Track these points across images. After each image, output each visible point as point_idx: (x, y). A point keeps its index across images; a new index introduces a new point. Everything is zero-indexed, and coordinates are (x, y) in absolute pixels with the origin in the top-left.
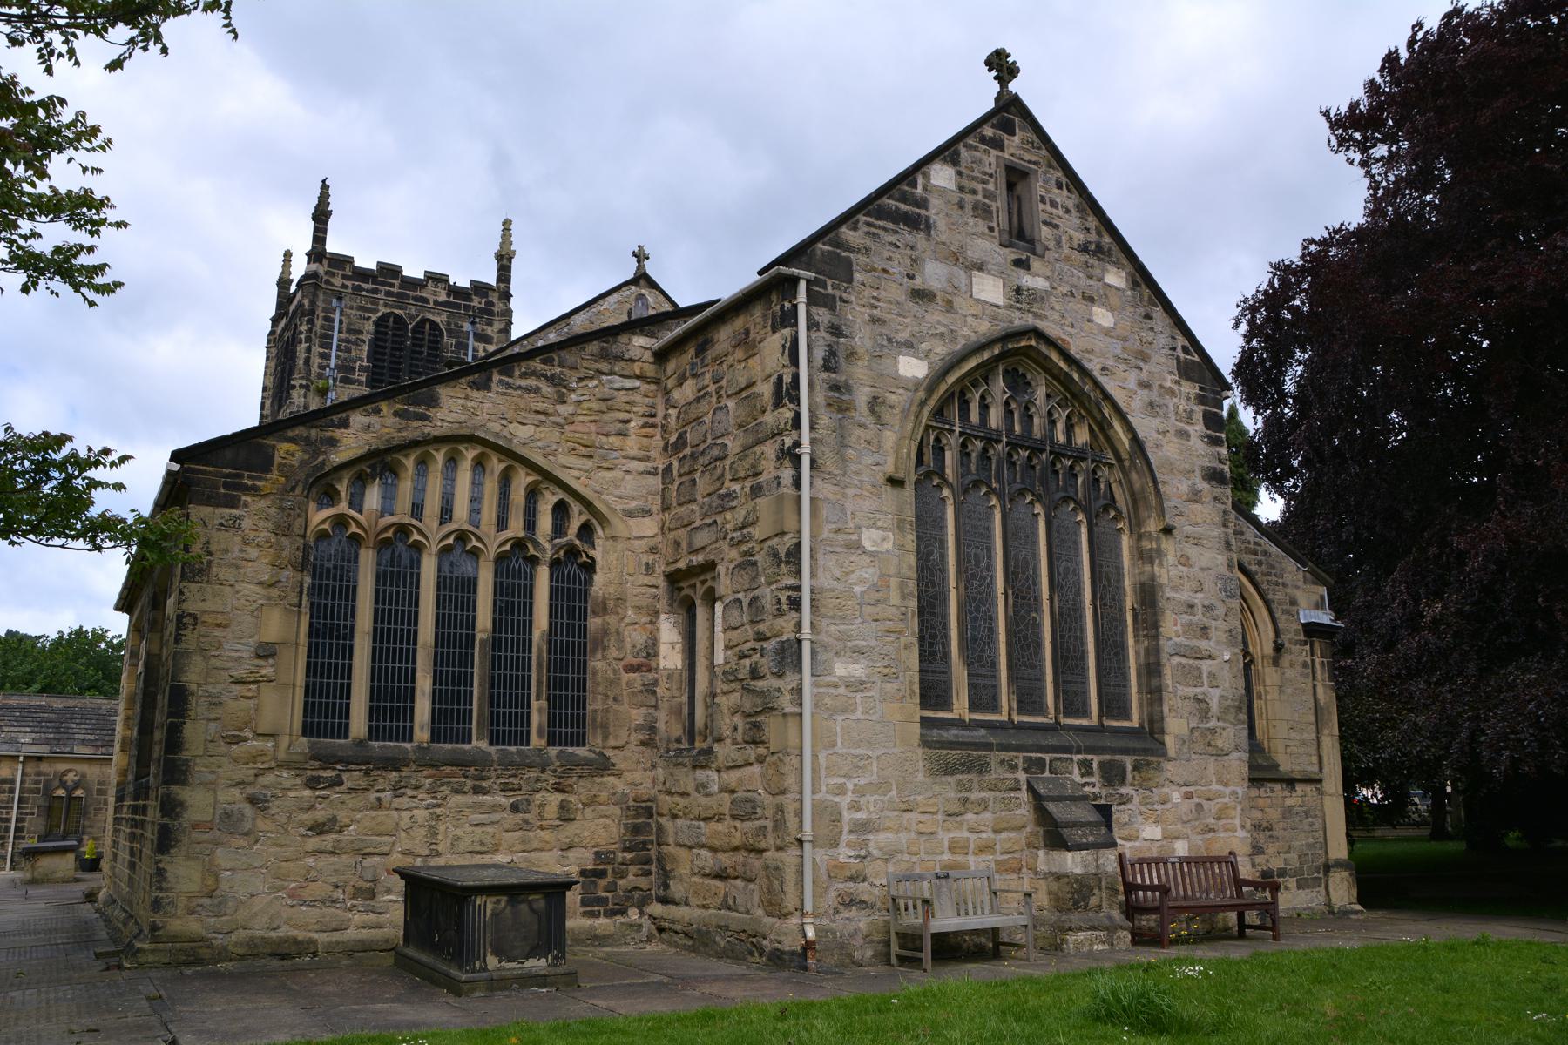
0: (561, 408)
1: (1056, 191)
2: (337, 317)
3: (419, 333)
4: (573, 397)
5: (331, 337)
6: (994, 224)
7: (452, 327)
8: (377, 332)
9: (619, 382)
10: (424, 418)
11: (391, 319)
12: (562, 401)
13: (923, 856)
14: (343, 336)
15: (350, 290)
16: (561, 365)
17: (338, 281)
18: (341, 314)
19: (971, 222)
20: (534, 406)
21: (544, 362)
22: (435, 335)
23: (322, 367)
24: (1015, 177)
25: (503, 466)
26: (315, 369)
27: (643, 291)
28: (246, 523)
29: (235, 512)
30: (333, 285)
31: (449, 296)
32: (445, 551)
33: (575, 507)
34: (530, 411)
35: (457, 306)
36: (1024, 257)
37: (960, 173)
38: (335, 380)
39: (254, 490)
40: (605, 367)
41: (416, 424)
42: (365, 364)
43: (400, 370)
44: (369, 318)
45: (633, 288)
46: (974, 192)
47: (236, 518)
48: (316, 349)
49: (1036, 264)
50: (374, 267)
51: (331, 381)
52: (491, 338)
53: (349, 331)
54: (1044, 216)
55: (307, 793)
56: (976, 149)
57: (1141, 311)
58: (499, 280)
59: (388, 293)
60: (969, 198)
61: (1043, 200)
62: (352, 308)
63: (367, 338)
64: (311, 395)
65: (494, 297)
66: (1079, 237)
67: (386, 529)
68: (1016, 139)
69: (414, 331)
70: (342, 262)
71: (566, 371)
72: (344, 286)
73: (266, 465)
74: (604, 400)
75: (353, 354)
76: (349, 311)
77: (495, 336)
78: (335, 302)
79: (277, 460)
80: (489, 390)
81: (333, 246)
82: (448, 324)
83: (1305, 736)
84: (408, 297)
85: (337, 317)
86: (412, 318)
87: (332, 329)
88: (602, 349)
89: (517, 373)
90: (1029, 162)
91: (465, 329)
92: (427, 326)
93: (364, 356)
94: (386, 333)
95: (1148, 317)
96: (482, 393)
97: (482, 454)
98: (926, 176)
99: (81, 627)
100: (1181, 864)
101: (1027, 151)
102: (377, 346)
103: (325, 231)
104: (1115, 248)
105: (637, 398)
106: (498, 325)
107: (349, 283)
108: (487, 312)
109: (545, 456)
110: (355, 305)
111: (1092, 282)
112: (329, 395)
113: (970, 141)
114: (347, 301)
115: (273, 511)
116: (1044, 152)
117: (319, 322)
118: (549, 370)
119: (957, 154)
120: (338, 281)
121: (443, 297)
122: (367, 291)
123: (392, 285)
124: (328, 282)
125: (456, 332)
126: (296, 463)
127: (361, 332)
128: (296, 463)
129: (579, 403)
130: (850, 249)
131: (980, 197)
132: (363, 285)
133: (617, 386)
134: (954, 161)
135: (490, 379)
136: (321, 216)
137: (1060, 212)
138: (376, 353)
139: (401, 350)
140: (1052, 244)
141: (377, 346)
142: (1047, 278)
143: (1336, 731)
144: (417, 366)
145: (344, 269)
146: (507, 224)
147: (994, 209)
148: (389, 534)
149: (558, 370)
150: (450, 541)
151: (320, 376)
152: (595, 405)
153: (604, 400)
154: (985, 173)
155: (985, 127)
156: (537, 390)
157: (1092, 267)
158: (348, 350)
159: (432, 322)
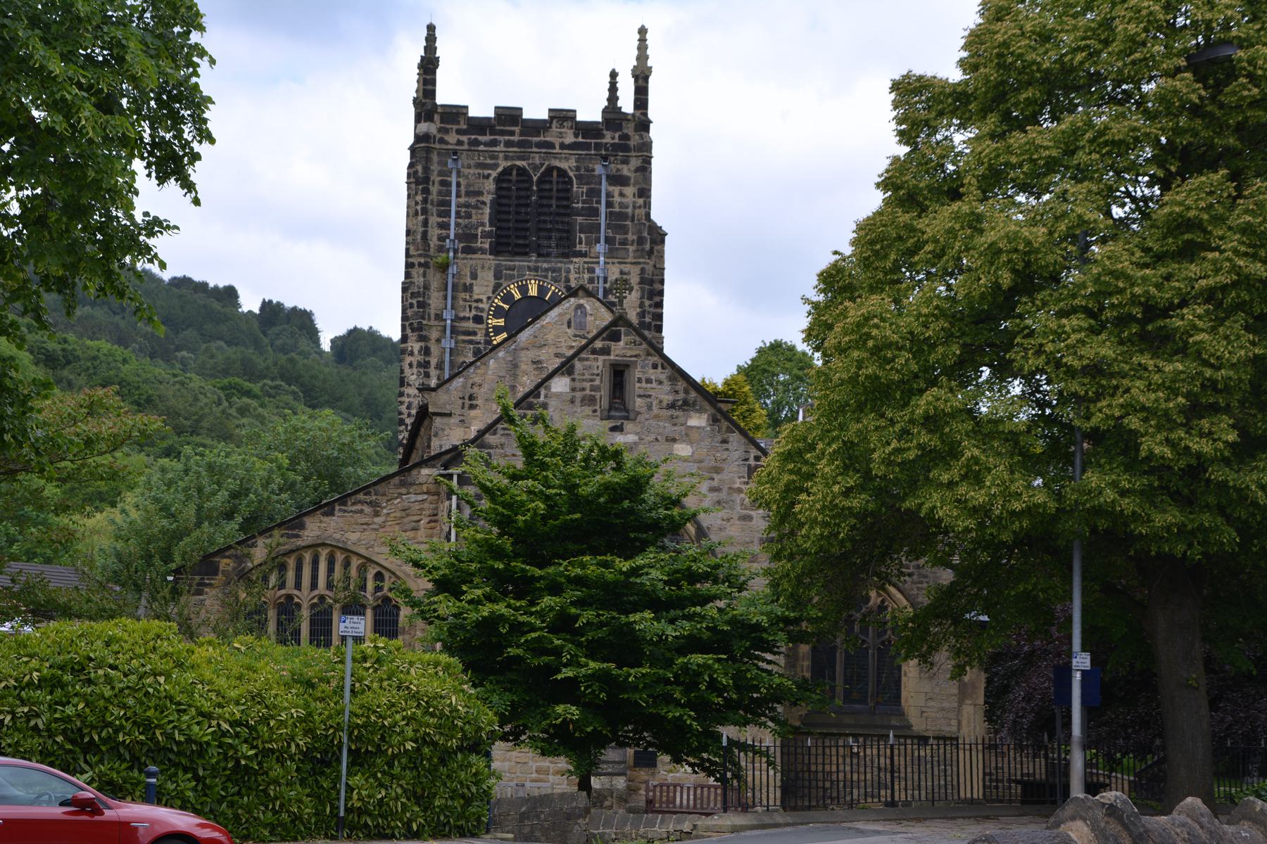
0: (377, 520)
1: (652, 371)
2: (454, 180)
3: (546, 182)
4: (385, 511)
5: (449, 204)
6: (597, 407)
7: (582, 172)
8: (498, 189)
9: (413, 498)
10: (297, 536)
11: (514, 172)
12: (377, 514)
13: (518, 774)
14: (462, 200)
15: (466, 147)
16: (376, 494)
17: (452, 138)
18: (459, 175)
19: (579, 410)
20: (360, 521)
21: (365, 494)
22: (565, 183)
23: (442, 239)
24: (619, 373)
25: (343, 556)
26: (434, 242)
27: (582, 301)
28: (207, 602)
29: (201, 597)
30: (447, 143)
31: (576, 136)
32: (313, 606)
33: (387, 575)
34: (357, 524)
35: (586, 146)
36: (619, 424)
37: (573, 380)
38: (455, 251)
39: (210, 585)
40: (403, 491)
41: (292, 540)
42: (488, 229)
43: (527, 229)
44: (488, 176)
45: (572, 300)
46: (583, 389)
47: (202, 600)
48: (434, 220)
49: (629, 426)
50: (491, 114)
51: (451, 254)
52: (628, 178)
53: (468, 194)
54: (638, 392)
56: (587, 359)
57: (719, 438)
58: (636, 107)
59: (509, 144)
60: (579, 395)
61: (640, 380)
62: (469, 167)
63: (488, 198)
64: (431, 272)
65: (629, 129)
66: (668, 398)
67: (280, 598)
68: (622, 343)
69: (540, 181)
70: (456, 114)
71: (379, 497)
72: (460, 143)
73: (214, 571)
74: (404, 510)
75: (474, 220)
76: (466, 171)
77: (632, 175)
78: (450, 164)
79: (221, 568)
80: (333, 515)
81: (445, 95)
82: (578, 169)
83: (946, 705)
84: (529, 144)
85: (454, 180)
86: (536, 168)
87: (449, 194)
88: (401, 481)
89: (349, 503)
90: (631, 356)
91: (597, 173)
92: (555, 174)
93: (486, 220)
94: (509, 189)
95: (725, 441)
96: (329, 518)
97: (332, 551)
98: (548, 388)
99: (371, 328)
100: (695, 789)
101: (630, 349)
102: (500, 205)
103: (433, 82)
104: (700, 399)
105: (426, 505)
106: (635, 163)
107: (465, 138)
108: (622, 147)
109: (367, 549)
110: (472, 163)
111: (676, 428)
112: (450, 271)
113: (583, 355)
114: (464, 160)
115: (220, 595)
116: (644, 346)
117: (434, 189)
118: (368, 498)
119: (573, 367)
120: (452, 138)
121: (570, 139)
122: (486, 144)
123: (512, 133)
124: (442, 141)
125: (587, 177)
126: (230, 569)
127: (480, 193)
128: (230, 569)
129: (389, 514)
130: (491, 447)
131: (588, 392)
132: (480, 138)
133: (412, 500)
134: (570, 372)
135: (333, 509)
136: (429, 65)
137: (654, 385)
138: (499, 212)
139: (527, 205)
140: (644, 410)
141: (500, 205)
142: (637, 434)
143: (981, 700)
144: (545, 222)
145: (458, 123)
146: (643, 31)
147: (598, 397)
148: (282, 600)
149: (374, 498)
150: (315, 600)
151: (441, 249)
152: (398, 514)
153: (404, 510)
154: (593, 374)
155: (597, 342)
156: (361, 511)
157: (677, 417)
158: (469, 216)
159: (559, 169)
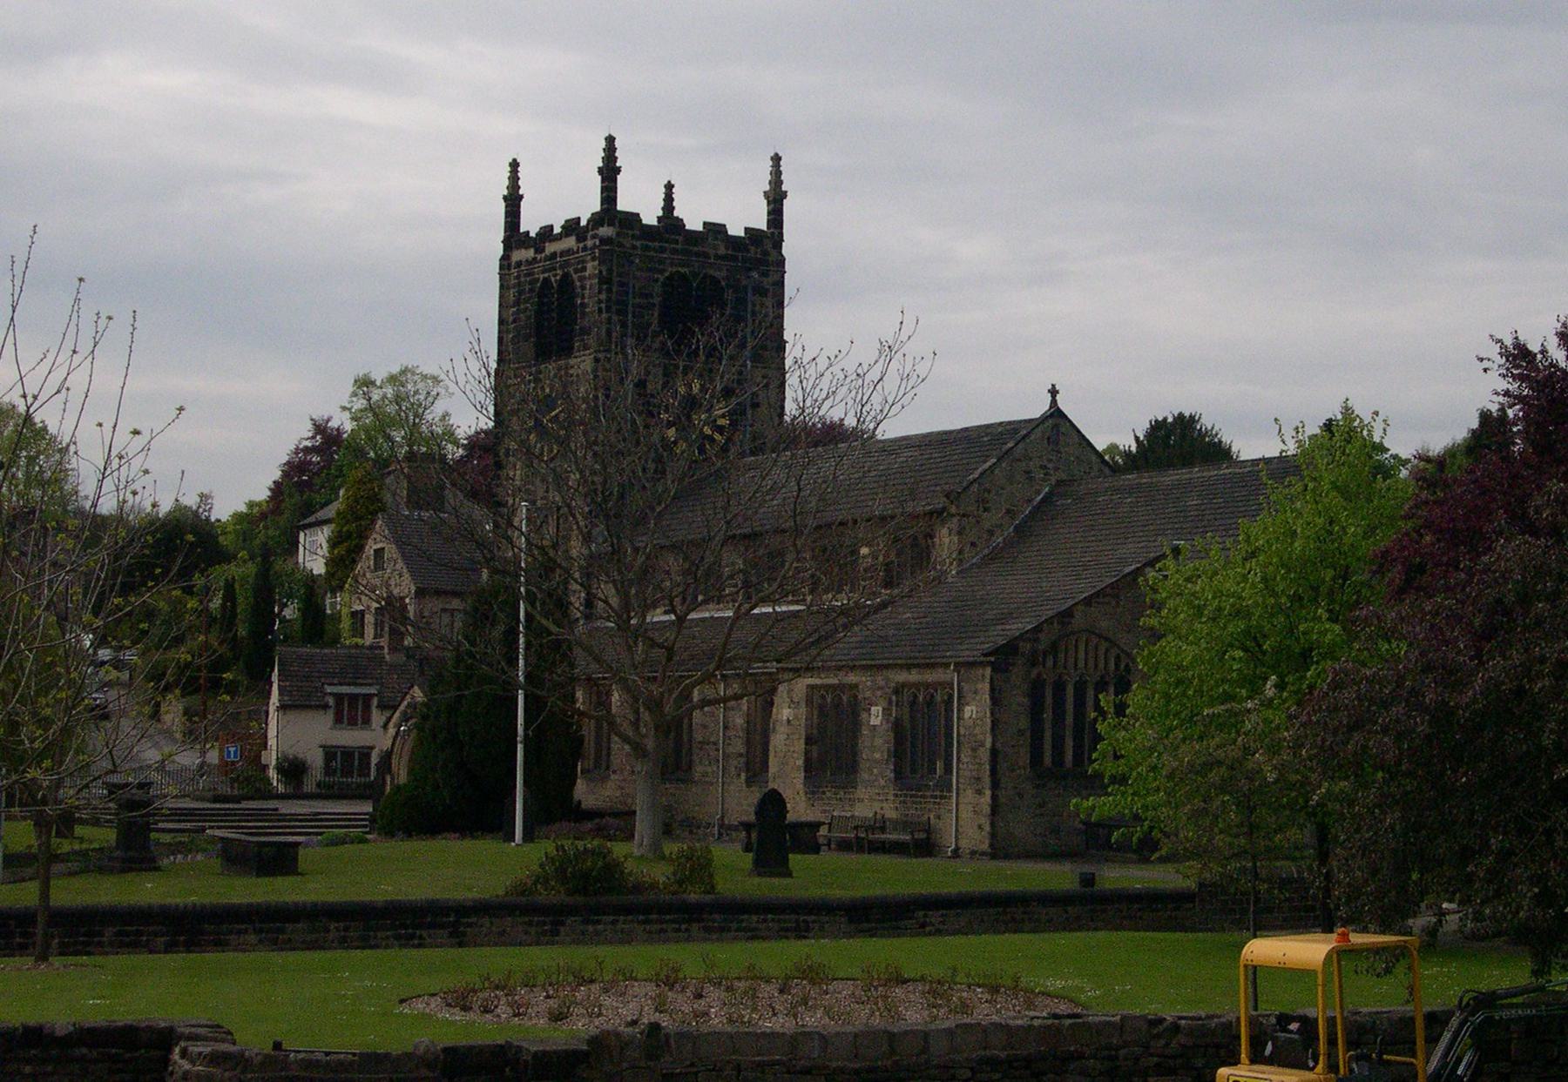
33: (1123, 656)
55: (1035, 790)
81: (623, 204)
121: (722, 251)
